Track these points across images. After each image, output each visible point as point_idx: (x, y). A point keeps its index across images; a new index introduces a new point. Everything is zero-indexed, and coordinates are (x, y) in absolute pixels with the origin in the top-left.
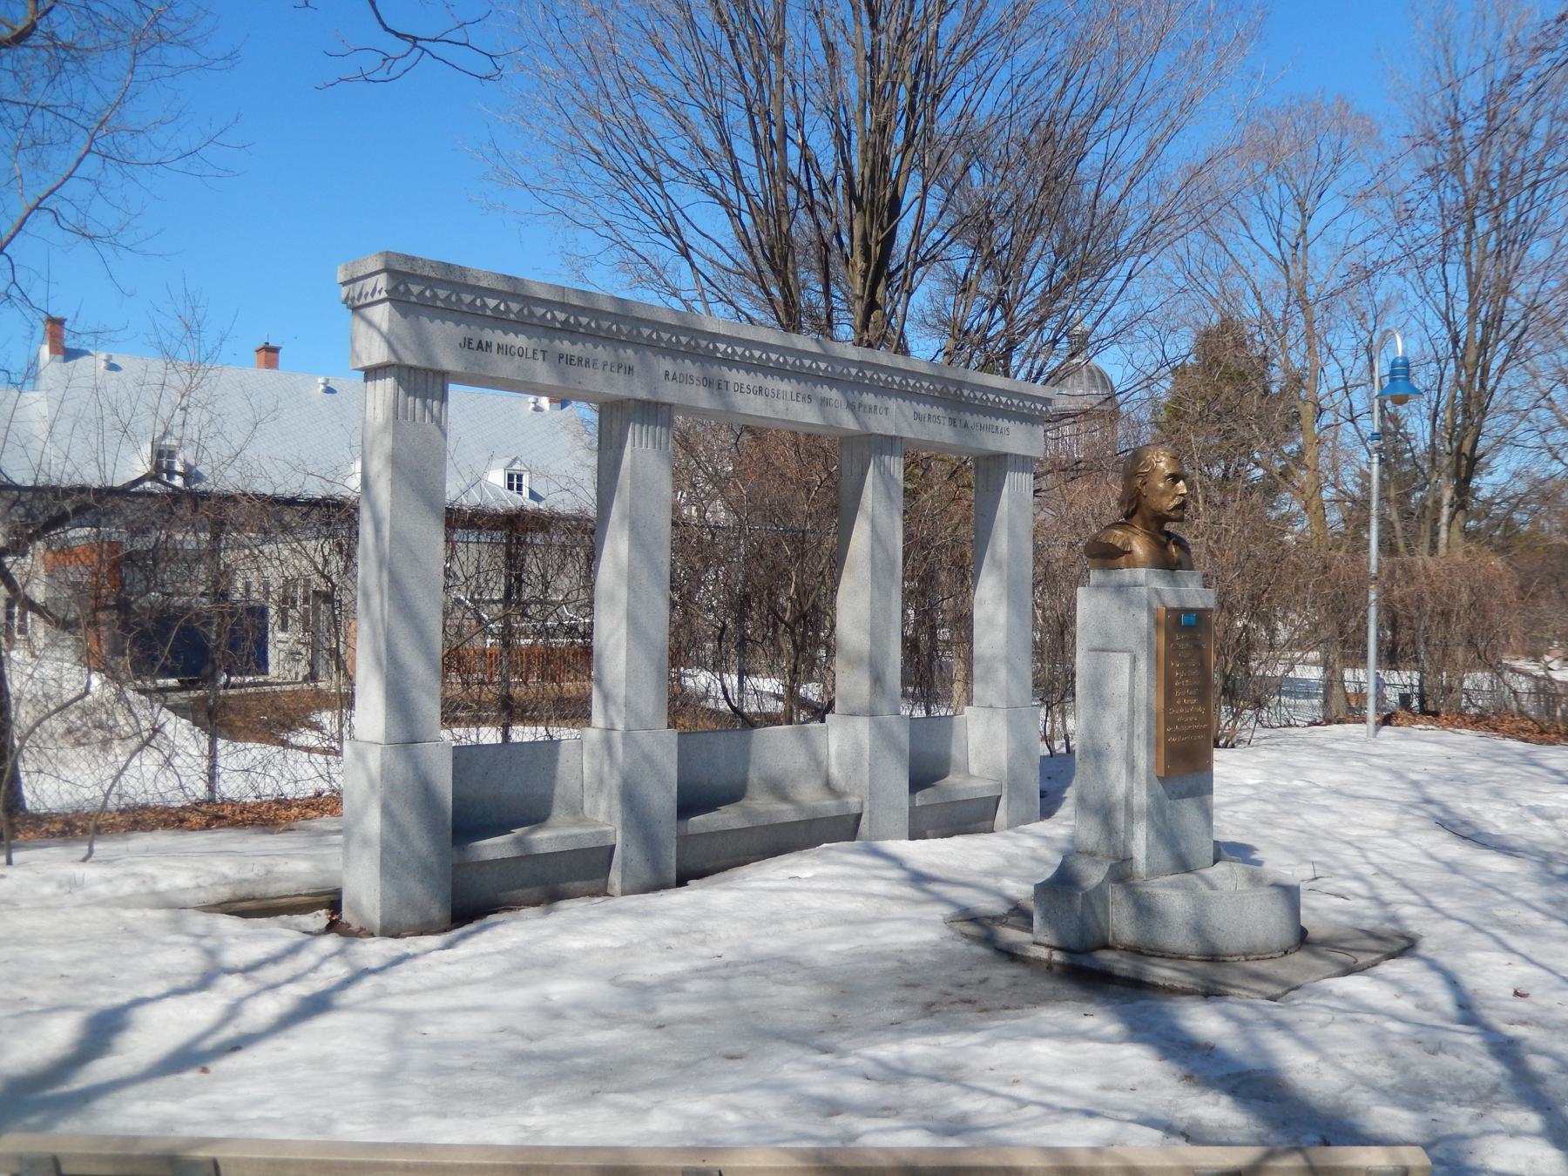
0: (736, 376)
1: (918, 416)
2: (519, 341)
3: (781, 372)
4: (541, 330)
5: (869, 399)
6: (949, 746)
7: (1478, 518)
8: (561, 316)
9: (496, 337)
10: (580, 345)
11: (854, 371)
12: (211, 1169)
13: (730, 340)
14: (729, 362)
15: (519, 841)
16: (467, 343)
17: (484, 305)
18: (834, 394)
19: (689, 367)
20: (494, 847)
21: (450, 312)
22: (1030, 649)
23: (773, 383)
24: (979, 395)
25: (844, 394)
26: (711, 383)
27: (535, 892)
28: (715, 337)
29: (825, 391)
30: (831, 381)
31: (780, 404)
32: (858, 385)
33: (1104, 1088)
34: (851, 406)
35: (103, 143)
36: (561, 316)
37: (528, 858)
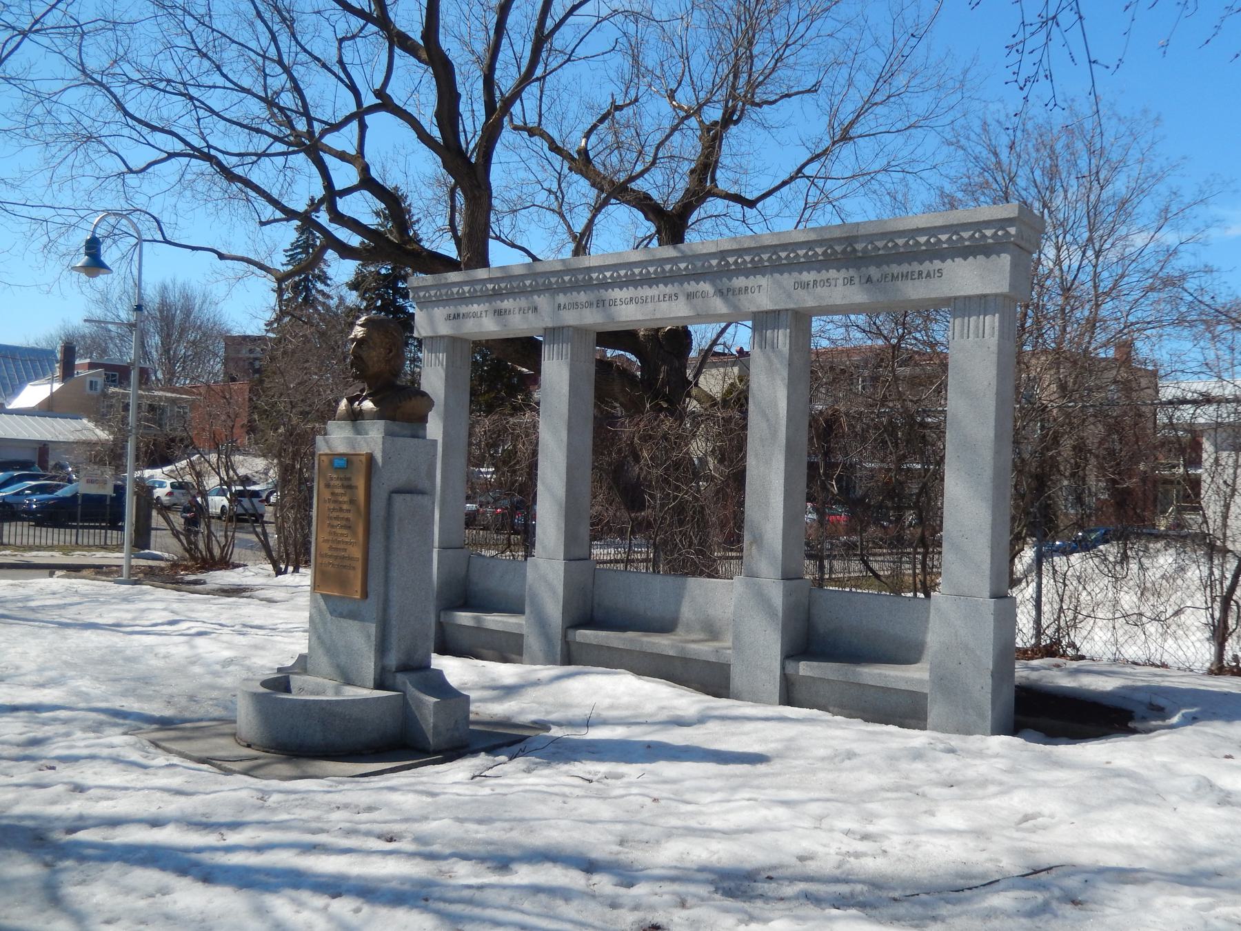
1: (805, 286)
2: (475, 308)
5: (740, 282)
6: (925, 632)
7: (825, 473)
8: (490, 286)
9: (463, 309)
11: (714, 262)
14: (604, 285)
15: (477, 619)
16: (448, 317)
18: (705, 287)
19: (582, 297)
20: (465, 618)
23: (646, 292)
24: (880, 244)
26: (601, 303)
27: (490, 653)
29: (692, 287)
30: (697, 276)
31: (1049, 221)
33: (164, 891)
34: (720, 293)
36: (490, 286)
37: (479, 629)
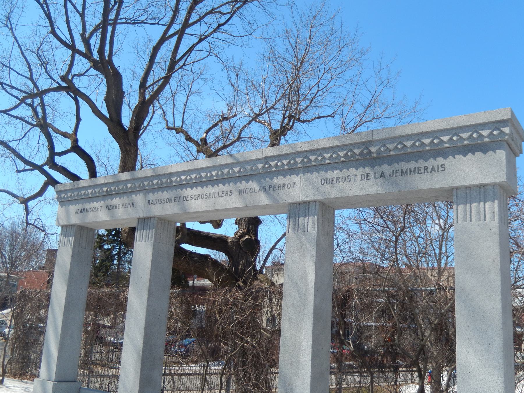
0: (190, 192)
3: (212, 182)
4: (101, 198)
5: (278, 180)
10: (227, 185)
11: (260, 166)
12: (64, 385)
13: (188, 172)
17: (481, 136)
18: (253, 185)
21: (118, 194)
22: (121, 363)
23: (209, 190)
25: (259, 182)
26: (178, 199)
28: (179, 174)
29: (243, 185)
30: (247, 177)
32: (269, 173)
35: (417, 116)
